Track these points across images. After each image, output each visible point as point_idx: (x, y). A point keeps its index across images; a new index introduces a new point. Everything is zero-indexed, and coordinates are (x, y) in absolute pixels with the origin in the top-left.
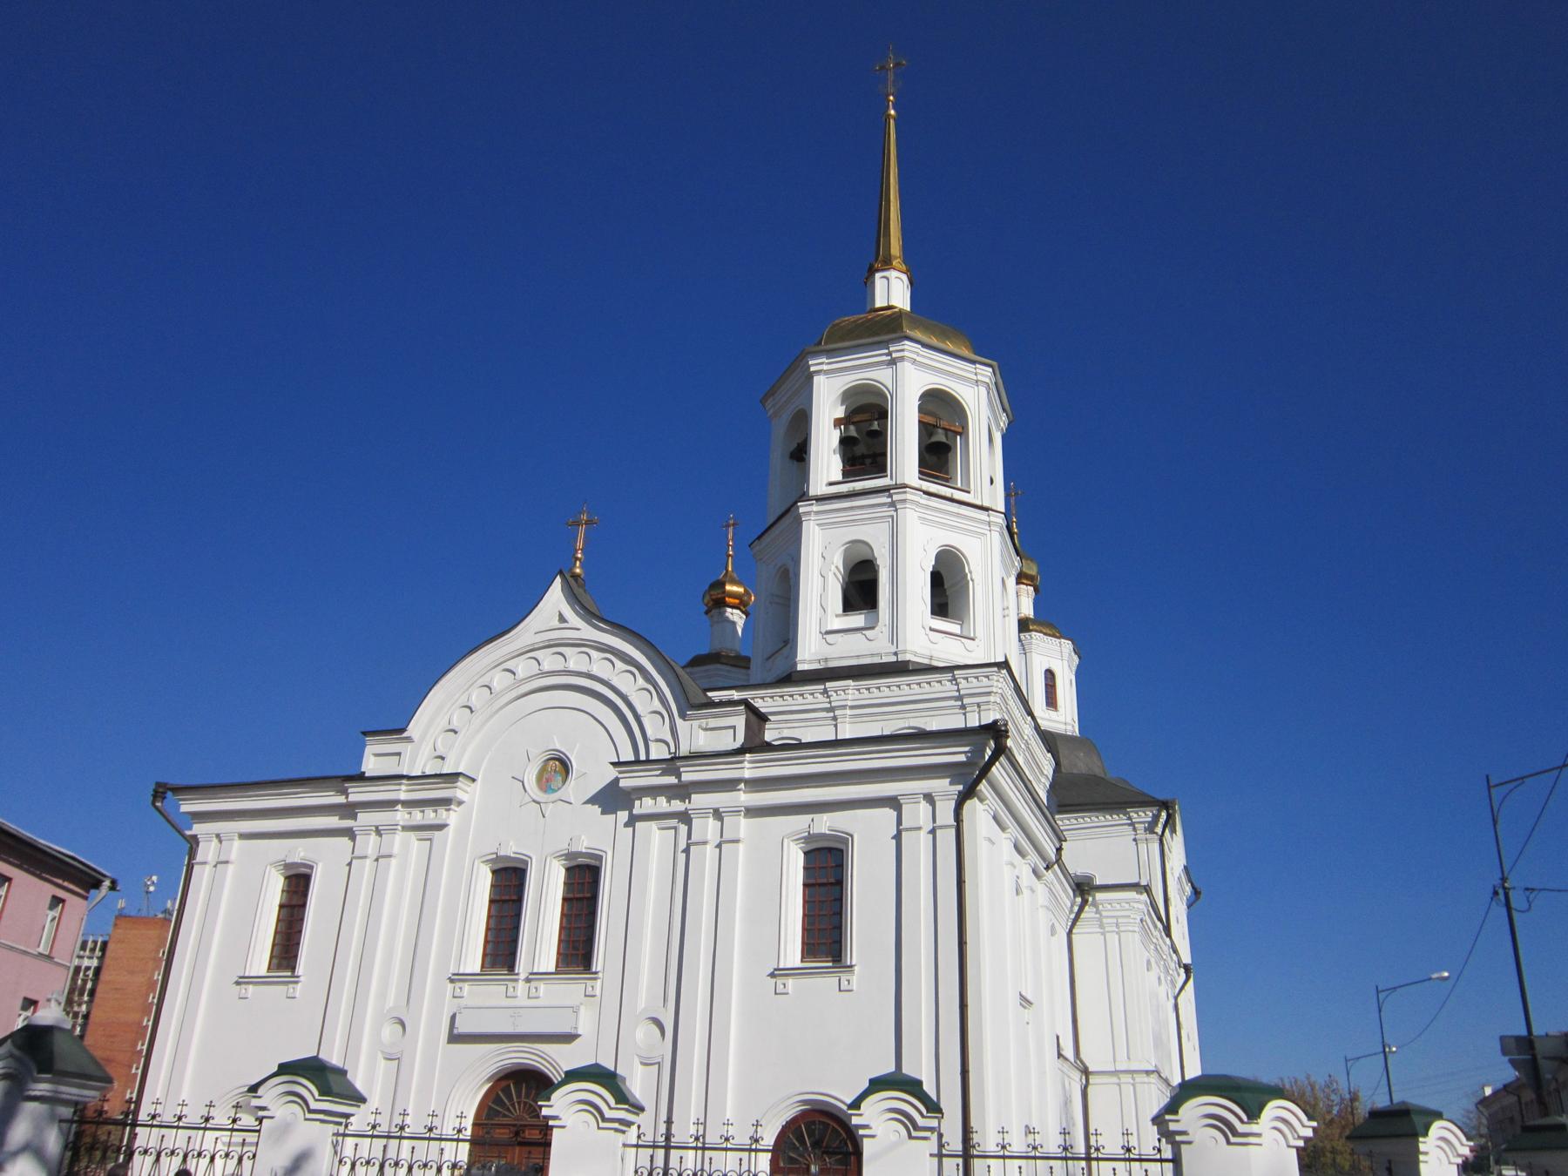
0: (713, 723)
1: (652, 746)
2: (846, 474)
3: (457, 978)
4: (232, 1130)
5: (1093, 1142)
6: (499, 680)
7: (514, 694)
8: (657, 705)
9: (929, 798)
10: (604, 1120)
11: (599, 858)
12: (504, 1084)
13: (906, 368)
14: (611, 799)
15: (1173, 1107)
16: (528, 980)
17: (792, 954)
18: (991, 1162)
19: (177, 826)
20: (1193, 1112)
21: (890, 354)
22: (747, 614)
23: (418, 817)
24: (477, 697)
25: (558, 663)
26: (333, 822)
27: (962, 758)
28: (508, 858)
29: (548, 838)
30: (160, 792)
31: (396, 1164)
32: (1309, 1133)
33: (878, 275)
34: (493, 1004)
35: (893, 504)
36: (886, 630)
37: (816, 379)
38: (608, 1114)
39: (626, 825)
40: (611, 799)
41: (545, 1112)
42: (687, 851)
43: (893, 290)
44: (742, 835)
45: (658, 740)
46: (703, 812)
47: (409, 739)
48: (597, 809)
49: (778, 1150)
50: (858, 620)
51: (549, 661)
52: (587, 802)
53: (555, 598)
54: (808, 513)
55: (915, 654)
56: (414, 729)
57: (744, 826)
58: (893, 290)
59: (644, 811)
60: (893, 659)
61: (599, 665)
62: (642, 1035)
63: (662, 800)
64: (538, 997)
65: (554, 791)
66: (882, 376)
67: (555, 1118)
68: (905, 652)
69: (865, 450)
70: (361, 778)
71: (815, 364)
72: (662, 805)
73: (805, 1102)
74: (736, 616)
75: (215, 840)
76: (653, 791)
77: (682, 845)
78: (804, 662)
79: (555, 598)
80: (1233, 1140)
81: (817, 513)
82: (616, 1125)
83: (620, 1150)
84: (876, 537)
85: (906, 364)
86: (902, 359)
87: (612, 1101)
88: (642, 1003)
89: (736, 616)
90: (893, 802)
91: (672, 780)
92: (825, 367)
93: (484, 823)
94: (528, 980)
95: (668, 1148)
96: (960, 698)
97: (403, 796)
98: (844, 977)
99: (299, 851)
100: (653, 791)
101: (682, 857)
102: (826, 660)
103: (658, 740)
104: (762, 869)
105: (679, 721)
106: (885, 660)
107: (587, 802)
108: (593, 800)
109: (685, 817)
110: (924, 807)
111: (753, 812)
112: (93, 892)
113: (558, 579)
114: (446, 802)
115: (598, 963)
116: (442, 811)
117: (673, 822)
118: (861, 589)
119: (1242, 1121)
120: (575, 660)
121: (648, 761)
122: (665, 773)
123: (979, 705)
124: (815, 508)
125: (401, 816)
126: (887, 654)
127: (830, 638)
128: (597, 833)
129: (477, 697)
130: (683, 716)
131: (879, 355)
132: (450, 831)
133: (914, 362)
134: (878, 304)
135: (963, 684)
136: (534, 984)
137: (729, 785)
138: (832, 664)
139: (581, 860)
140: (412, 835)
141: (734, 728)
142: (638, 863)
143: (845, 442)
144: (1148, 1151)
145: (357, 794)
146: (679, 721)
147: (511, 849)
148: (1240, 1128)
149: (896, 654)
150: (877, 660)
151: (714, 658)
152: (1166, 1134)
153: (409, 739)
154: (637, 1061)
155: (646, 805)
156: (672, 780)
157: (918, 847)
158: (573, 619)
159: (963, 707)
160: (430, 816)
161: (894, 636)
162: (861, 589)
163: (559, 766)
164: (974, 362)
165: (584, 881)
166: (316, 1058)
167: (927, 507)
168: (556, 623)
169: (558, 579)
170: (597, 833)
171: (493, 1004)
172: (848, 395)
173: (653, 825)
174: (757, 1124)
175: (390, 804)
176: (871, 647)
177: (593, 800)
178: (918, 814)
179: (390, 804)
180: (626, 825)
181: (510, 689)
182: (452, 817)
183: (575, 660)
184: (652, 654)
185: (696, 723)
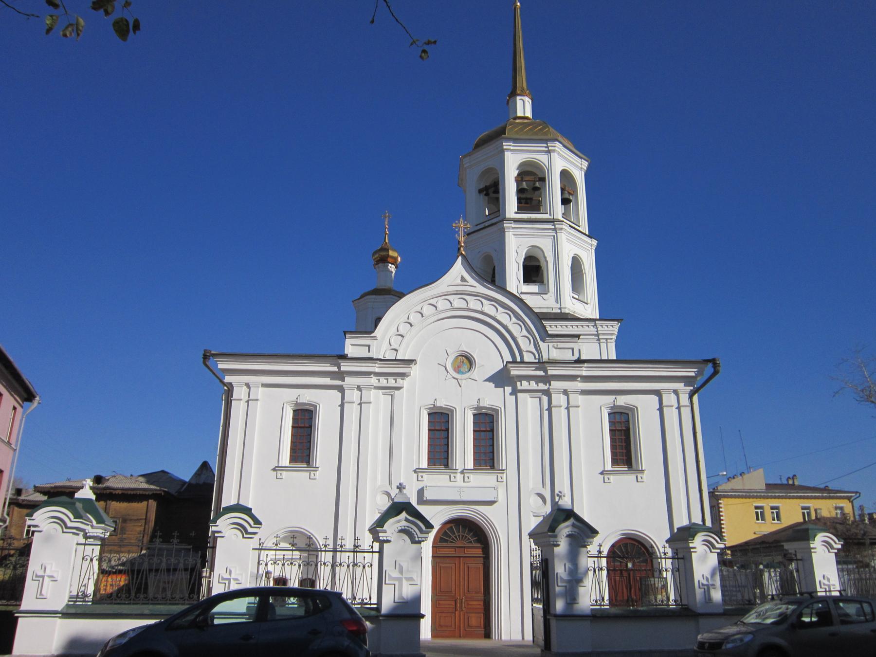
0: (561, 345)
1: (525, 354)
2: (519, 208)
4: (85, 544)
5: (339, 542)
6: (427, 310)
7: (436, 318)
8: (525, 332)
9: (676, 392)
10: (67, 527)
12: (449, 526)
14: (501, 379)
15: (381, 522)
16: (462, 472)
18: (366, 554)
19: (219, 376)
20: (392, 526)
21: (547, 147)
23: (383, 382)
24: (414, 318)
25: (463, 305)
26: (327, 381)
27: (693, 374)
29: (465, 398)
30: (206, 357)
31: (340, 564)
32: (840, 546)
33: (518, 98)
35: (555, 229)
37: (506, 153)
38: (70, 524)
39: (511, 394)
40: (501, 379)
41: (691, 545)
42: (549, 409)
43: (524, 107)
44: (580, 404)
45: (527, 351)
46: (557, 391)
47: (375, 338)
48: (492, 385)
49: (608, 557)
51: (458, 302)
52: (486, 380)
53: (458, 268)
54: (509, 228)
57: (581, 399)
58: (524, 107)
59: (523, 388)
60: (559, 311)
63: (533, 383)
65: (463, 373)
66: (543, 158)
67: (694, 548)
68: (565, 308)
69: (531, 196)
70: (344, 357)
71: (506, 145)
72: (533, 385)
73: (623, 534)
74: (392, 268)
75: (245, 387)
76: (528, 378)
79: (458, 268)
80: (65, 530)
81: (514, 228)
82: (74, 531)
83: (75, 546)
84: (545, 244)
85: (556, 154)
86: (554, 151)
87: (72, 517)
88: (531, 486)
89: (392, 268)
90: (658, 393)
91: (541, 373)
92: (512, 148)
93: (424, 389)
94: (462, 472)
95: (335, 551)
96: (598, 335)
97: (377, 370)
98: (639, 476)
99: (307, 397)
100: (528, 378)
101: (546, 413)
103: (527, 351)
105: (541, 343)
106: (554, 311)
107: (486, 380)
108: (489, 380)
109: (547, 393)
110: (673, 397)
111: (584, 392)
112: (26, 403)
113: (460, 258)
114: (403, 375)
116: (399, 379)
117: (540, 395)
118: (533, 271)
119: (251, 527)
120: (474, 304)
121: (522, 362)
122: (537, 369)
123: (606, 340)
124: (513, 226)
125: (373, 381)
128: (492, 397)
129: (414, 318)
130: (543, 340)
131: (542, 147)
135: (600, 328)
136: (466, 475)
137: (573, 378)
139: (484, 411)
140: (380, 392)
141: (573, 349)
144: (366, 547)
145: (346, 367)
146: (541, 343)
147: (442, 403)
148: (250, 530)
149: (560, 309)
150: (550, 311)
151: (377, 292)
152: (376, 539)
153: (375, 338)
154: (532, 514)
155: (525, 385)
156: (541, 373)
157: (671, 415)
158: (471, 281)
159: (599, 340)
160: (392, 382)
161: (558, 299)
162: (533, 271)
163: (466, 361)
164: (581, 158)
165: (486, 424)
166: (238, 504)
167: (570, 233)
168: (459, 281)
169: (460, 258)
170: (492, 397)
172: (522, 165)
173: (528, 395)
174: (600, 546)
175: (367, 374)
177: (489, 380)
179: (367, 374)
180: (511, 394)
181: (433, 315)
182: (405, 383)
184: (522, 305)
185: (551, 345)
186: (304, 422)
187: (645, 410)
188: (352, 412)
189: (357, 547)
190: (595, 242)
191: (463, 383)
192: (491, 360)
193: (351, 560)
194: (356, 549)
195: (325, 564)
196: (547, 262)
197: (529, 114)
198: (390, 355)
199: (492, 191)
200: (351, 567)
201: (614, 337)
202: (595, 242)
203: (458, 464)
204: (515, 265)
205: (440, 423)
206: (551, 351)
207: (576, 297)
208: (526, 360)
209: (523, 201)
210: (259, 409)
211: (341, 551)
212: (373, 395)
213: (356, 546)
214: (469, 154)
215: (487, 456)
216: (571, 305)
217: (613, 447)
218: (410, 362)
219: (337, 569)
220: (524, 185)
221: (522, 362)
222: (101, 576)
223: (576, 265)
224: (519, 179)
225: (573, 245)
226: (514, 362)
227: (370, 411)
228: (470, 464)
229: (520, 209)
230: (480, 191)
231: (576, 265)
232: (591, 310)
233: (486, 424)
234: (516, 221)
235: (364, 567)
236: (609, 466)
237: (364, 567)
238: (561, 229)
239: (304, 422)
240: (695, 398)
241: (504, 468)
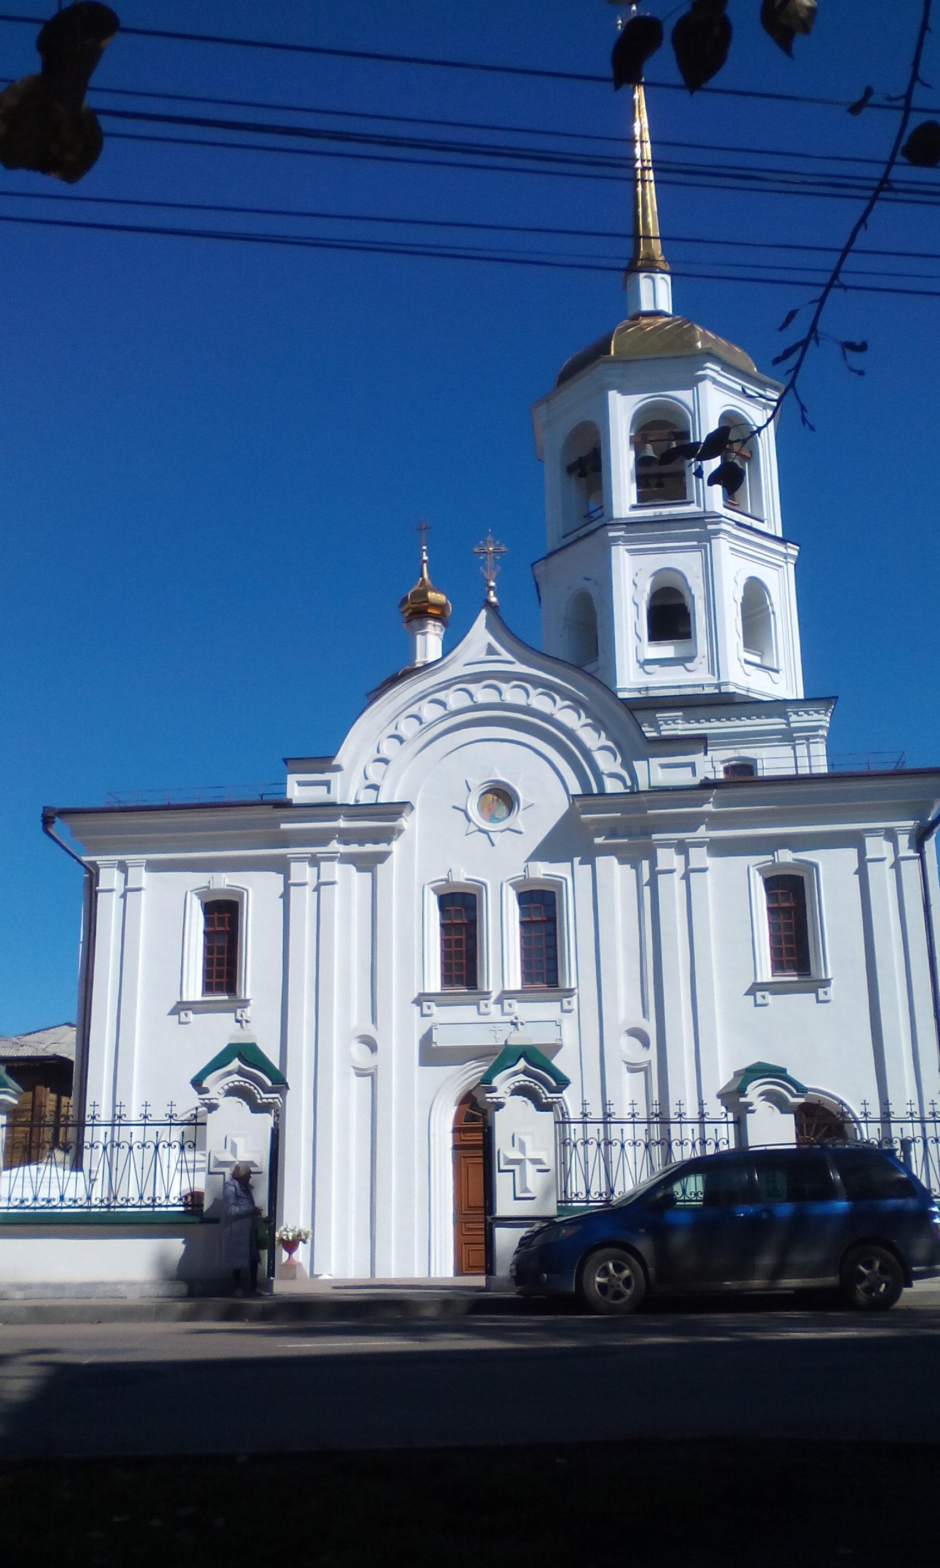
2: (641, 497)
3: (422, 999)
11: (559, 885)
13: (706, 387)
16: (499, 1001)
17: (194, 990)
22: (445, 624)
23: (354, 848)
24: (407, 728)
28: (459, 884)
31: (92, 1146)
33: (642, 275)
34: (463, 1024)
36: (705, 661)
42: (653, 884)
43: (656, 293)
47: (338, 768)
50: (666, 650)
55: (736, 686)
56: (343, 757)
61: (539, 702)
62: (625, 1048)
64: (504, 1013)
65: (499, 820)
68: (726, 684)
77: (646, 876)
78: (624, 690)
84: (687, 563)
95: (702, 1123)
102: (647, 689)
104: (725, 899)
106: (708, 690)
113: (483, 613)
115: (569, 980)
118: (670, 616)
120: (512, 695)
123: (807, 738)
126: (710, 685)
127: (647, 668)
132: (394, 860)
133: (715, 382)
134: (646, 306)
138: (653, 693)
142: (602, 895)
143: (641, 462)
147: (462, 875)
150: (699, 691)
153: (338, 768)
157: (881, 877)
158: (507, 656)
160: (369, 848)
161: (714, 666)
162: (670, 616)
163: (502, 797)
165: (541, 908)
169: (483, 613)
171: (463, 1024)
176: (693, 678)
178: (877, 847)
183: (512, 695)
186: (223, 917)
187: (833, 872)
188: (303, 900)
189: (585, 1115)
190: (793, 551)
191: (496, 838)
192: (546, 795)
193: (697, 1136)
194: (117, 1122)
195: (118, 1145)
196: (693, 597)
197: (665, 304)
198: (367, 797)
199: (589, 466)
200: (108, 1149)
201: (823, 732)
202: (793, 551)
203: (491, 981)
204: (631, 609)
205: (460, 912)
206: (655, 773)
207: (757, 660)
208: (609, 789)
209: (653, 481)
210: (143, 903)
211: (93, 1125)
212: (335, 871)
213: (702, 1115)
214: (546, 399)
215: (544, 965)
216: (741, 675)
217: (775, 939)
218: (396, 810)
219: (86, 1153)
220: (649, 451)
221: (602, 794)
222: (228, 1171)
223: (755, 601)
224: (640, 437)
225: (745, 561)
226: (587, 794)
227: (334, 897)
228: (515, 981)
229: (644, 499)
230: (570, 469)
231: (755, 601)
232: (787, 683)
233: (541, 908)
234: (631, 525)
235: (131, 1148)
236: (766, 974)
237: (131, 1148)
238: (717, 532)
239: (223, 917)
240: (930, 845)
241: (573, 985)
